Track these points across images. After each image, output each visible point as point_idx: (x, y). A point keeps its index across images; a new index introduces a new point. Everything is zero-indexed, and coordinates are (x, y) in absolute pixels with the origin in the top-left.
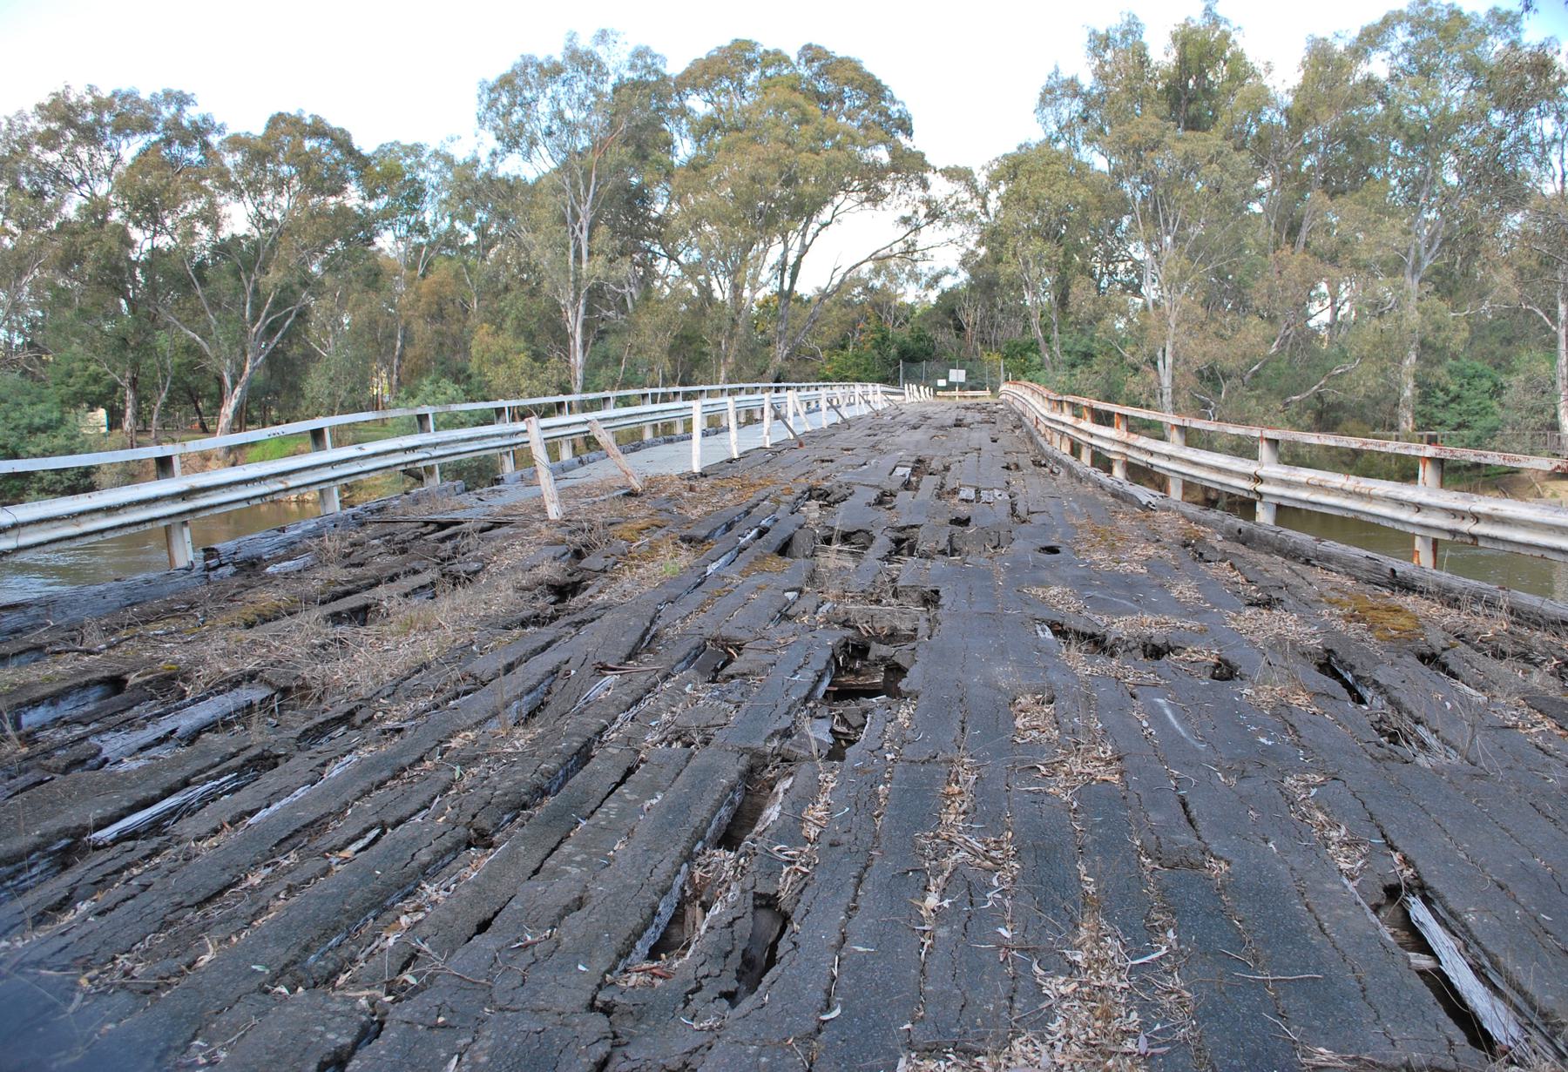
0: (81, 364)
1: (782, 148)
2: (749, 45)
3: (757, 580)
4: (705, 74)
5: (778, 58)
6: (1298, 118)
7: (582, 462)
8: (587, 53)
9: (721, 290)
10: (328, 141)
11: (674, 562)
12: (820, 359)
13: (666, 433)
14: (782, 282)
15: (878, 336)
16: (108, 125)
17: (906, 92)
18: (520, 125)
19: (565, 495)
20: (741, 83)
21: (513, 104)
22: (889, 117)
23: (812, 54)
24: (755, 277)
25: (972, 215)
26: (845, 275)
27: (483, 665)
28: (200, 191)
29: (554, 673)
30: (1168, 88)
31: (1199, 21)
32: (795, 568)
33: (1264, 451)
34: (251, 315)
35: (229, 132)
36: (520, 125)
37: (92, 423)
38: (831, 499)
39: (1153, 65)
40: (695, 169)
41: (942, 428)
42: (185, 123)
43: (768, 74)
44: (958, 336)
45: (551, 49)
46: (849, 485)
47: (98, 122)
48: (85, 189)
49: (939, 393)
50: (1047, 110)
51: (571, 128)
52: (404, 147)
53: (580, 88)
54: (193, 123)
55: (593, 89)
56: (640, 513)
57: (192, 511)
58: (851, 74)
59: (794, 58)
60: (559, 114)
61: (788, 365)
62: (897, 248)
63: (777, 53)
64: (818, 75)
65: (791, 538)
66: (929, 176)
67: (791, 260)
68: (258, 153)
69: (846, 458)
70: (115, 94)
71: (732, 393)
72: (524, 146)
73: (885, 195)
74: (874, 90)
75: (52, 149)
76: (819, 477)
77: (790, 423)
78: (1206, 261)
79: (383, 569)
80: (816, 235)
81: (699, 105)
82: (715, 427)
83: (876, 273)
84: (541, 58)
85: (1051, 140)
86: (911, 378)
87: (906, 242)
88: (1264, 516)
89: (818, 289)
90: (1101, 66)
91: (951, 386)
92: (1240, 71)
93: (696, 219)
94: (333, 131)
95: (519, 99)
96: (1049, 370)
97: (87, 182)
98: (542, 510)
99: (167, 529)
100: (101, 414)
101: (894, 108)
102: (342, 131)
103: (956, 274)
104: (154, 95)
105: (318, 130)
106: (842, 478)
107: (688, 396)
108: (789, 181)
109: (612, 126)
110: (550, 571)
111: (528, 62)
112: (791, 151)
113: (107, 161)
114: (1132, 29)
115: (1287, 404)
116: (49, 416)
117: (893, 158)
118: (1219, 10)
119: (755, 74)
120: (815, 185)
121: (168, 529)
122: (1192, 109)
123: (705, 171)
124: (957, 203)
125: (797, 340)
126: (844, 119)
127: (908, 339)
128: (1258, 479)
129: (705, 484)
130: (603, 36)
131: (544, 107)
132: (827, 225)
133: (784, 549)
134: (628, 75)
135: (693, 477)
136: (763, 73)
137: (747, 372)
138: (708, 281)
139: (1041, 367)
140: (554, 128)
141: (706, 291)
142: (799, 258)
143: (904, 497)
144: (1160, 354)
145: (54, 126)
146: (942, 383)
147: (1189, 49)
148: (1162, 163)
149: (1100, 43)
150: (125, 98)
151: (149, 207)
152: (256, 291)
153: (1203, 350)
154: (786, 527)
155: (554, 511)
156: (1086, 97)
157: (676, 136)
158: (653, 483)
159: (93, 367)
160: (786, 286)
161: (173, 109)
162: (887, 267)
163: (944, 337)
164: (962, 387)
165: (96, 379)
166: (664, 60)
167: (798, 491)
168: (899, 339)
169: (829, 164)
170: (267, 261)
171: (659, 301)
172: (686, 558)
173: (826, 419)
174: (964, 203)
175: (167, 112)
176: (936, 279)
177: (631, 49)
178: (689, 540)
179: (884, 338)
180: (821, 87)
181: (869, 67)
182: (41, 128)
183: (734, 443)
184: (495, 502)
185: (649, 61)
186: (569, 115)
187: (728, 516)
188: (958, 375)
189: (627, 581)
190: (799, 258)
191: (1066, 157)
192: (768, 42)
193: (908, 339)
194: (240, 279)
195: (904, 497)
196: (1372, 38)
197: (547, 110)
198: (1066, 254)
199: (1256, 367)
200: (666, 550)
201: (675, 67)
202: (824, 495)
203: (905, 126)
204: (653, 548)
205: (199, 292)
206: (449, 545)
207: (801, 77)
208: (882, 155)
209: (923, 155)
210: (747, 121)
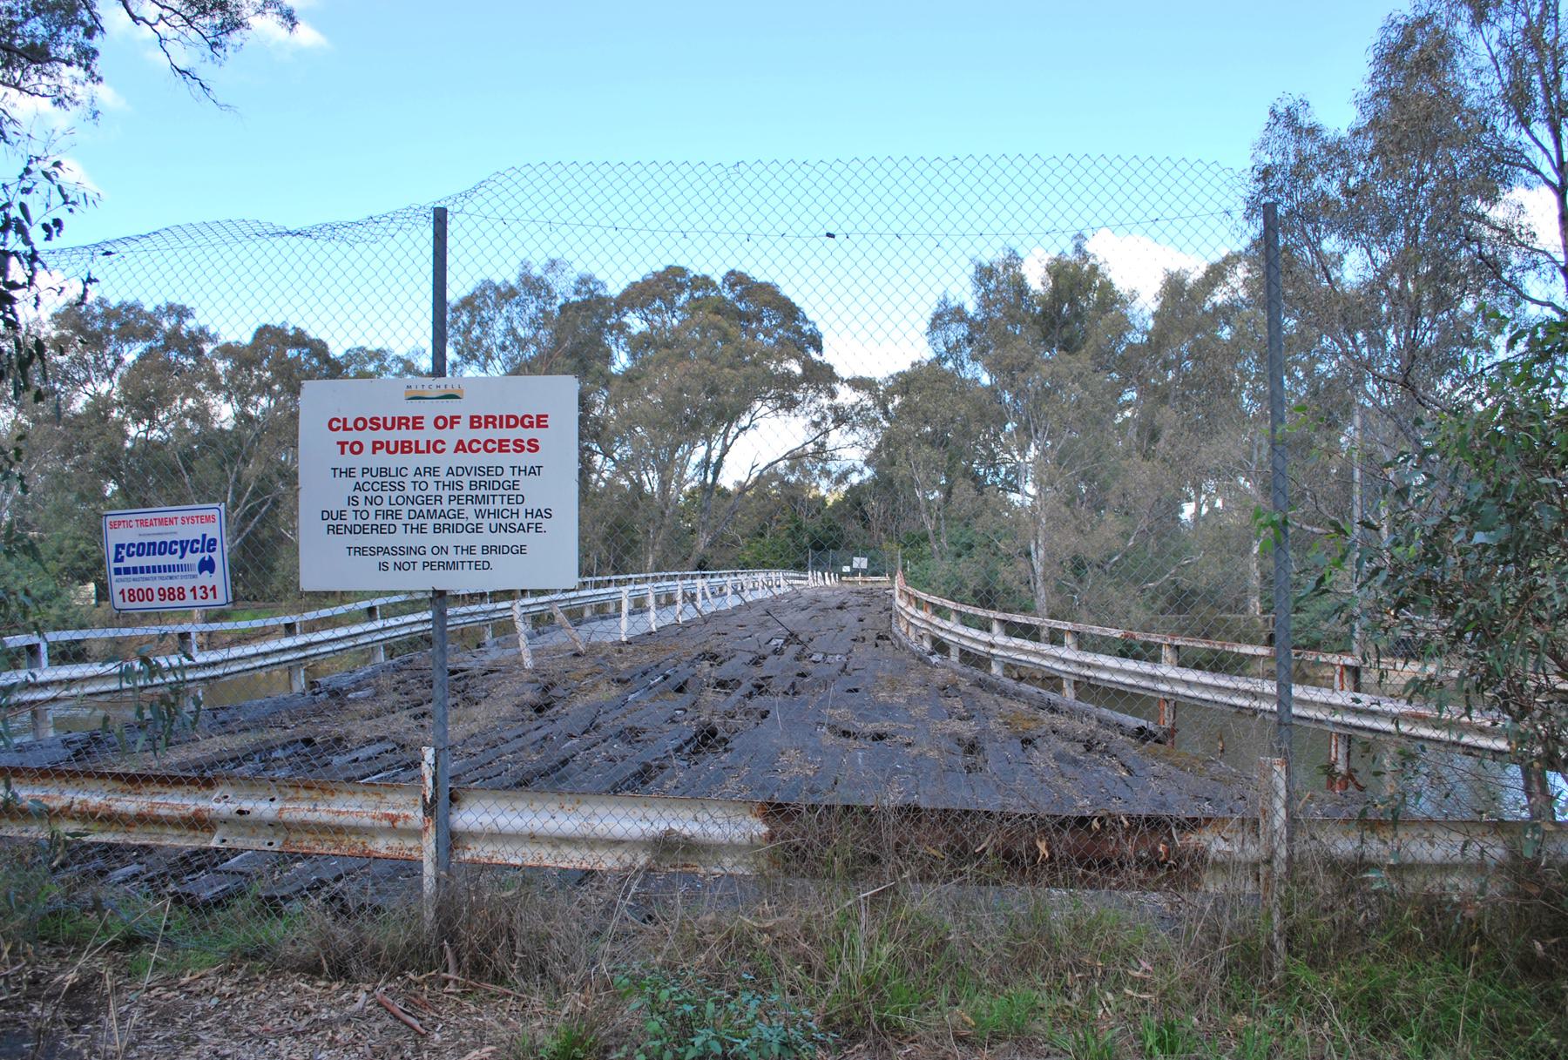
0: (71, 542)
1: (706, 364)
2: (682, 271)
3: (659, 704)
4: (639, 295)
5: (706, 282)
6: (1158, 340)
7: (539, 634)
8: (538, 280)
9: (651, 481)
10: (306, 350)
11: (607, 693)
12: (739, 545)
13: (601, 611)
14: (706, 478)
15: (792, 526)
16: (113, 333)
17: (816, 310)
18: (479, 340)
19: (535, 654)
20: (672, 302)
21: (472, 323)
22: (802, 335)
23: (736, 279)
24: (681, 475)
25: (875, 420)
26: (762, 471)
27: (507, 735)
28: (191, 392)
29: (544, 738)
30: (1043, 313)
31: (1071, 256)
32: (685, 699)
33: (996, 627)
34: (232, 501)
35: (222, 341)
36: (479, 340)
37: (83, 595)
38: (719, 660)
39: (1031, 293)
40: (631, 381)
41: (825, 610)
42: (183, 332)
43: (696, 295)
44: (864, 527)
45: (508, 275)
46: (733, 650)
47: (107, 331)
48: (89, 387)
49: (844, 578)
50: (937, 333)
51: (522, 343)
52: (369, 352)
53: (532, 309)
54: (190, 332)
55: (543, 311)
56: (585, 666)
57: (306, 657)
58: (768, 298)
59: (719, 281)
60: (512, 331)
61: (709, 552)
62: (810, 448)
63: (706, 278)
64: (740, 298)
65: (686, 682)
66: (837, 386)
67: (714, 459)
68: (243, 357)
69: (741, 632)
70: (121, 307)
71: (655, 579)
72: (482, 359)
73: (797, 403)
74: (789, 312)
75: (62, 354)
76: (713, 645)
77: (699, 606)
78: (1071, 466)
79: (424, 696)
80: (736, 437)
81: (635, 323)
82: (639, 607)
83: (792, 469)
84: (498, 281)
85: (940, 359)
86: (818, 565)
87: (816, 444)
88: (996, 670)
89: (739, 483)
90: (986, 294)
91: (854, 573)
92: (1109, 299)
93: (629, 421)
94: (312, 341)
95: (478, 319)
96: (938, 558)
97: (90, 380)
98: (521, 663)
99: (291, 667)
100: (91, 587)
101: (806, 328)
102: (320, 341)
103: (861, 472)
104: (158, 308)
105: (300, 339)
106: (729, 646)
107: (618, 583)
108: (713, 391)
109: (559, 343)
110: (530, 696)
111: (488, 285)
112: (714, 367)
113: (110, 363)
114: (1013, 260)
115: (1143, 591)
116: (45, 588)
117: (804, 370)
118: (1089, 247)
119: (685, 296)
120: (734, 396)
121: (290, 668)
122: (1066, 333)
123: (639, 382)
124: (862, 409)
125: (719, 530)
126: (762, 337)
127: (819, 529)
128: (992, 646)
129: (630, 649)
130: (553, 264)
131: (500, 325)
132: (745, 429)
133: (680, 690)
134: (574, 298)
135: (623, 644)
136: (692, 295)
137: (673, 559)
138: (639, 476)
139: (931, 555)
140: (508, 343)
141: (638, 486)
142: (722, 456)
143: (772, 659)
144: (1033, 547)
145: (67, 333)
146: (846, 569)
147: (1061, 281)
148: (1034, 381)
149: (984, 274)
150: (130, 309)
151: (144, 404)
152: (238, 480)
153: (1070, 541)
154: (684, 672)
155: (528, 662)
156: (971, 322)
157: (614, 348)
158: (593, 649)
159: (82, 546)
160: (710, 480)
161: (173, 321)
162: (801, 464)
163: (854, 527)
164: (864, 573)
165: (83, 556)
166: (604, 286)
167: (695, 654)
168: (811, 529)
169: (747, 378)
170: (250, 455)
171: (595, 494)
172: (615, 691)
173: (732, 601)
174: (869, 409)
175: (166, 324)
176: (844, 476)
177: (574, 276)
178: (619, 681)
179: (798, 528)
180: (742, 306)
181: (786, 291)
182: (54, 334)
183: (653, 620)
184: (493, 655)
185: (592, 287)
186: (521, 332)
187: (644, 667)
188: (861, 562)
189: (579, 703)
190: (722, 456)
191: (951, 375)
192: (697, 268)
193: (819, 529)
194: (223, 470)
195: (772, 659)
196: (1217, 274)
197: (502, 328)
198: (950, 459)
199: (1116, 558)
200: (603, 686)
201: (614, 289)
202: (714, 657)
203: (816, 342)
204: (595, 686)
205: (187, 479)
206: (462, 683)
207: (724, 299)
208: (795, 368)
209: (831, 368)
210: (676, 340)
